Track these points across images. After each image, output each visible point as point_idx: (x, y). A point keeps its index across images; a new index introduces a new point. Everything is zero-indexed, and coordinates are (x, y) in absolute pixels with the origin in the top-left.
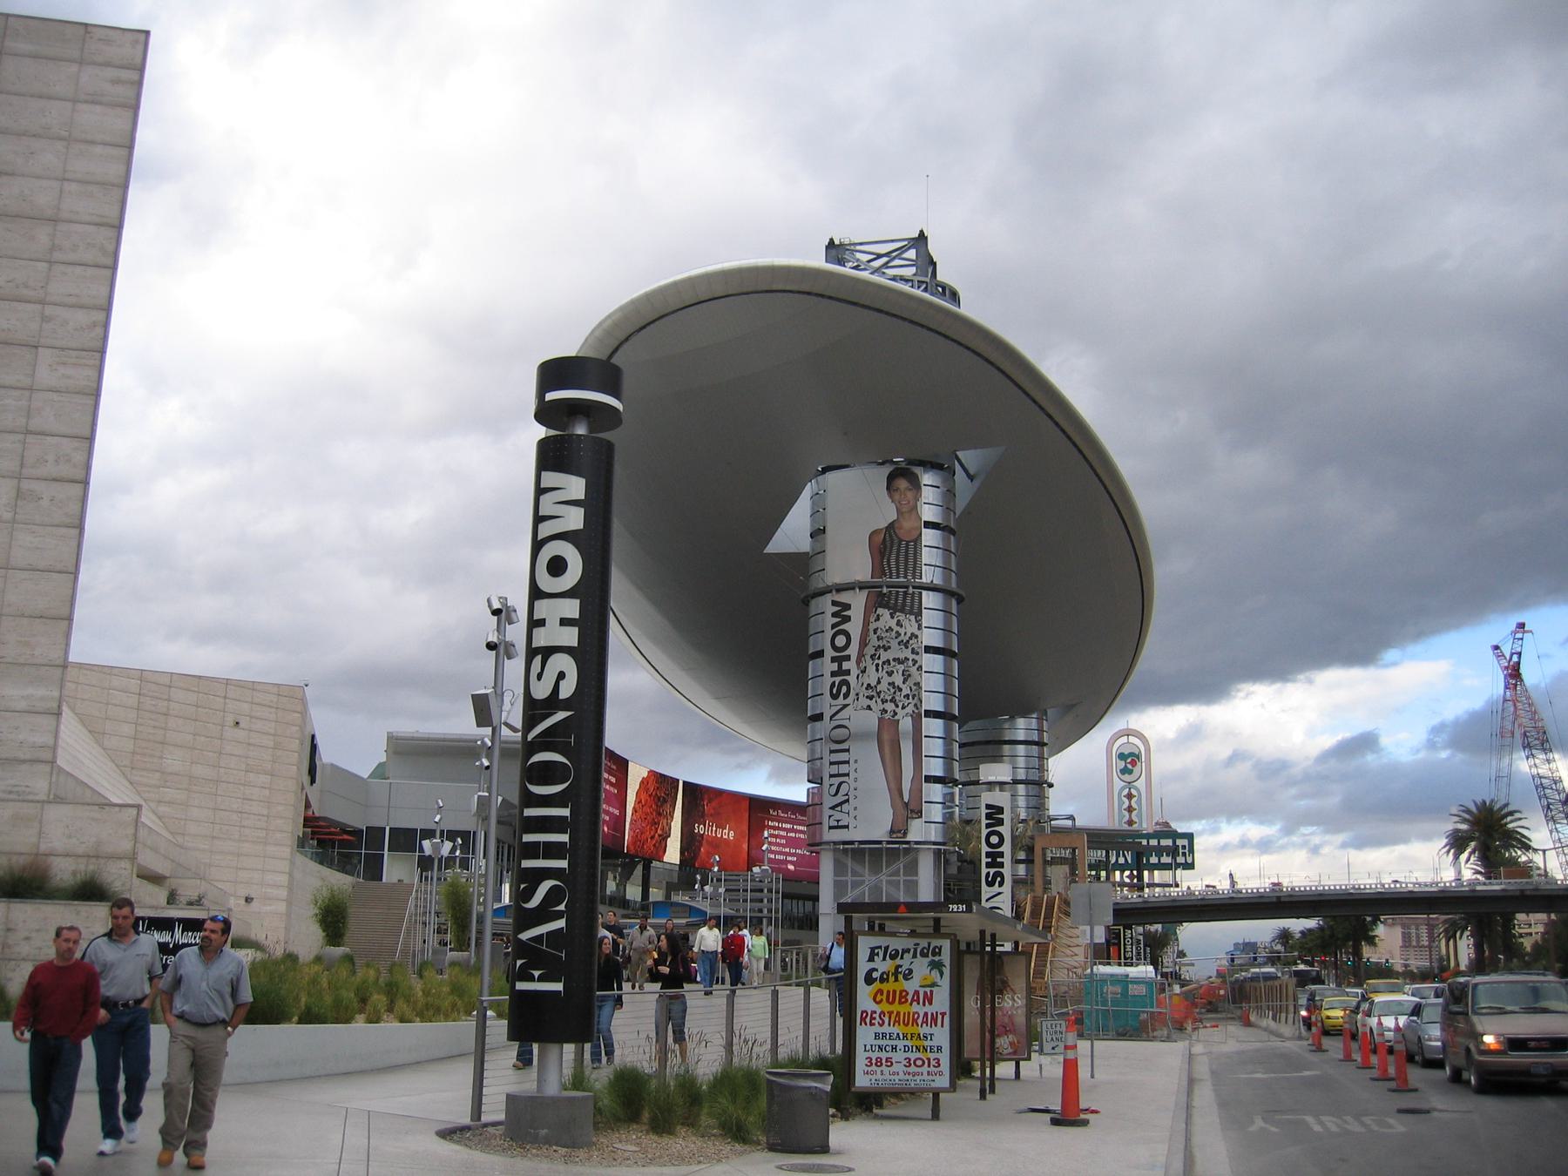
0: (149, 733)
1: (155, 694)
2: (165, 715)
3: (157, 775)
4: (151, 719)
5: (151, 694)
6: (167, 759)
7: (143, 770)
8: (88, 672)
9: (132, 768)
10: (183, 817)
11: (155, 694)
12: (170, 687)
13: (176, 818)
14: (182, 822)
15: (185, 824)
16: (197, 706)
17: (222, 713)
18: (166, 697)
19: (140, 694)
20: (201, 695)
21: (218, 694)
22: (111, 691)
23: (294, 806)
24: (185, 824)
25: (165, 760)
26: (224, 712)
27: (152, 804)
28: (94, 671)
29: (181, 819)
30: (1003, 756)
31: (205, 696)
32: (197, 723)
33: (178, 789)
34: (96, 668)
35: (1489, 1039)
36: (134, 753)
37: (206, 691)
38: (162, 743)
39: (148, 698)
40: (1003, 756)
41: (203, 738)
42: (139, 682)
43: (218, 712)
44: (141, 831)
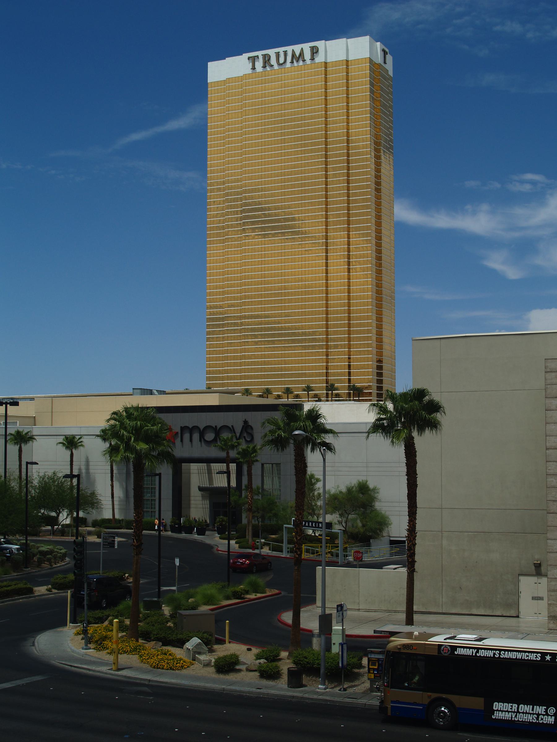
30: (229, 551)
40: (229, 551)
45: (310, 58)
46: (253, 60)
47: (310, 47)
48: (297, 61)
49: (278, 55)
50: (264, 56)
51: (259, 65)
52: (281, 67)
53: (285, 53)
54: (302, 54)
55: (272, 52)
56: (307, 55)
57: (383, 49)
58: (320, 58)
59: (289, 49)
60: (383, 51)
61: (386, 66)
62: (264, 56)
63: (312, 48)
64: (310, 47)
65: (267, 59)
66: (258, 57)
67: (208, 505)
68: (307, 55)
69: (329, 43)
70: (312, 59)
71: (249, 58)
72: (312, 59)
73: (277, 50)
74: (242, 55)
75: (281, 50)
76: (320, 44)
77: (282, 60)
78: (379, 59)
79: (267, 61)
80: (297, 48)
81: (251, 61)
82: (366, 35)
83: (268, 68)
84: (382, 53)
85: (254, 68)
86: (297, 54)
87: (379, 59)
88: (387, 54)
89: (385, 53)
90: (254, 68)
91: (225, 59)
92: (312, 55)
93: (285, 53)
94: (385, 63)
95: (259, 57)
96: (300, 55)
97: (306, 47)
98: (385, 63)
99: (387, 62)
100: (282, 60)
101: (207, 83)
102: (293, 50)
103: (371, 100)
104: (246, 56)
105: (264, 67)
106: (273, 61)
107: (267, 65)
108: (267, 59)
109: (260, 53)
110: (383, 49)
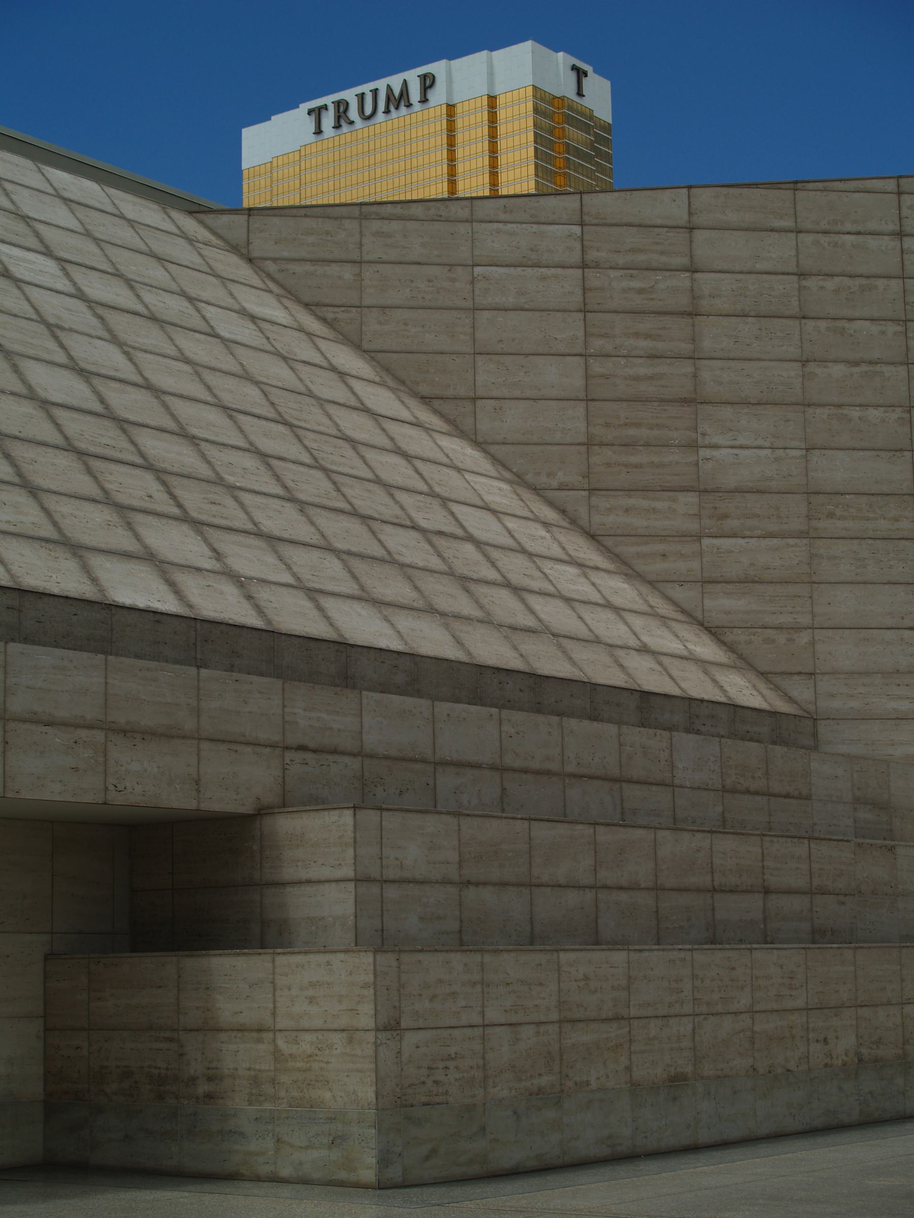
0: (636, 378)
1: (641, 257)
2: (690, 314)
3: (688, 501)
4: (637, 335)
5: (621, 260)
6: (716, 447)
7: (630, 491)
8: (395, 226)
9: (592, 490)
10: (805, 620)
11: (641, 257)
12: (691, 229)
13: (779, 628)
14: (804, 638)
15: (813, 643)
16: (802, 275)
17: (895, 285)
18: (684, 261)
19: (584, 266)
20: (808, 238)
21: (871, 226)
22: (477, 270)
23: (6, 643)
24: (813, 643)
25: (704, 453)
26: (693, 270)
27: (678, 593)
28: (411, 219)
29: (798, 628)
30: (283, 884)
31: (824, 239)
32: (810, 324)
33: (771, 535)
34: (417, 210)
35: (612, 276)
36: (590, 443)
37: (824, 225)
38: (685, 401)
39: (613, 274)
40: (283, 884)
41: (838, 370)
42: (577, 229)
43: (881, 283)
44: (624, 677)
45: (419, 100)
46: (317, 113)
47: (418, 76)
48: (397, 108)
49: (361, 97)
50: (338, 104)
51: (328, 120)
52: (372, 122)
53: (375, 92)
54: (405, 93)
55: (349, 95)
56: (415, 94)
57: (574, 65)
58: (438, 96)
59: (381, 84)
60: (572, 69)
61: (587, 102)
62: (338, 104)
63: (424, 77)
64: (418, 76)
65: (342, 109)
66: (325, 107)
67: (245, 187)
68: (415, 94)
69: (457, 63)
70: (424, 100)
71: (310, 112)
72: (424, 100)
73: (359, 90)
74: (298, 107)
75: (366, 88)
76: (437, 68)
77: (368, 110)
78: (565, 86)
79: (342, 115)
80: (395, 82)
81: (313, 117)
82: (527, 40)
83: (345, 128)
84: (573, 76)
85: (319, 131)
86: (397, 92)
87: (565, 86)
88: (586, 76)
89: (580, 74)
90: (319, 131)
91: (270, 119)
92: (423, 91)
93: (375, 92)
94: (580, 94)
95: (329, 108)
96: (401, 95)
97: (412, 76)
98: (580, 94)
99: (585, 91)
100: (368, 110)
101: (240, 172)
102: (388, 85)
103: (540, 174)
104: (305, 107)
105: (337, 126)
106: (353, 113)
107: (343, 122)
108: (342, 109)
109: (328, 100)
110: (574, 65)
